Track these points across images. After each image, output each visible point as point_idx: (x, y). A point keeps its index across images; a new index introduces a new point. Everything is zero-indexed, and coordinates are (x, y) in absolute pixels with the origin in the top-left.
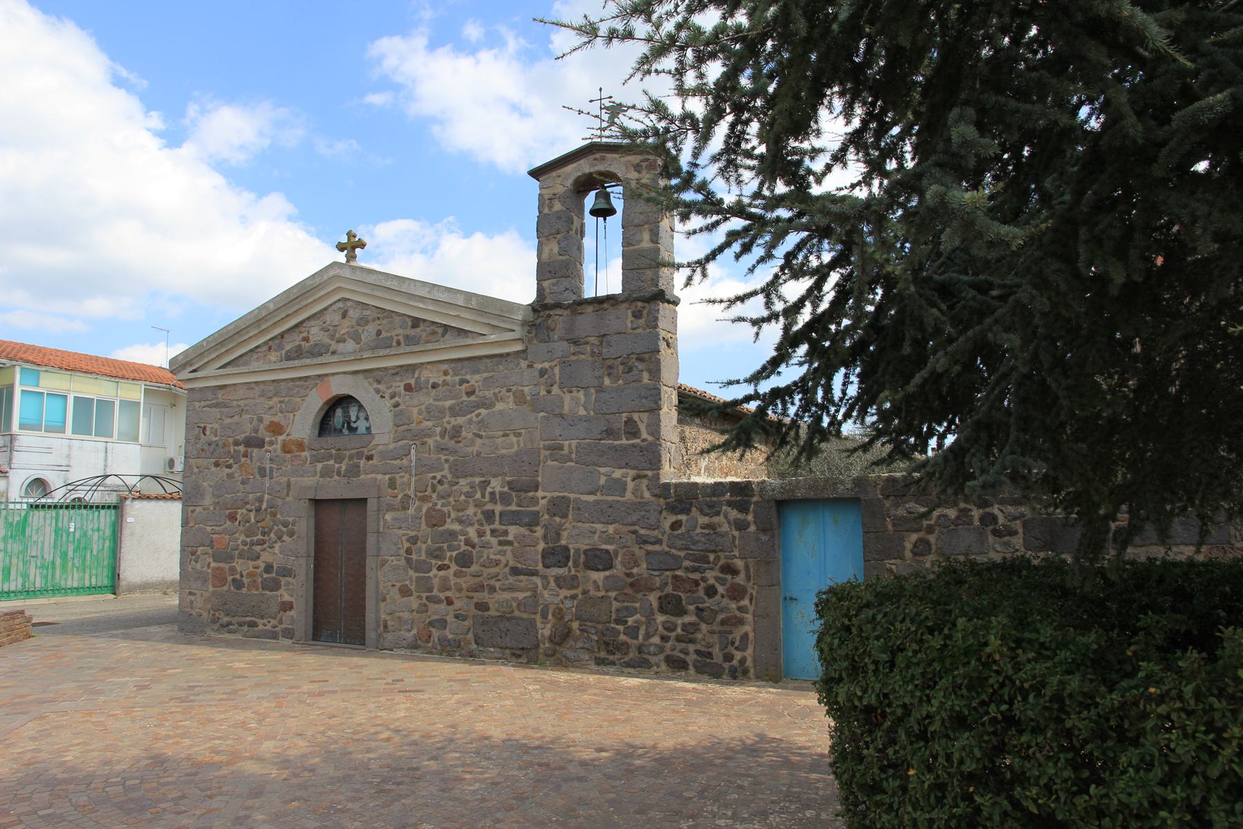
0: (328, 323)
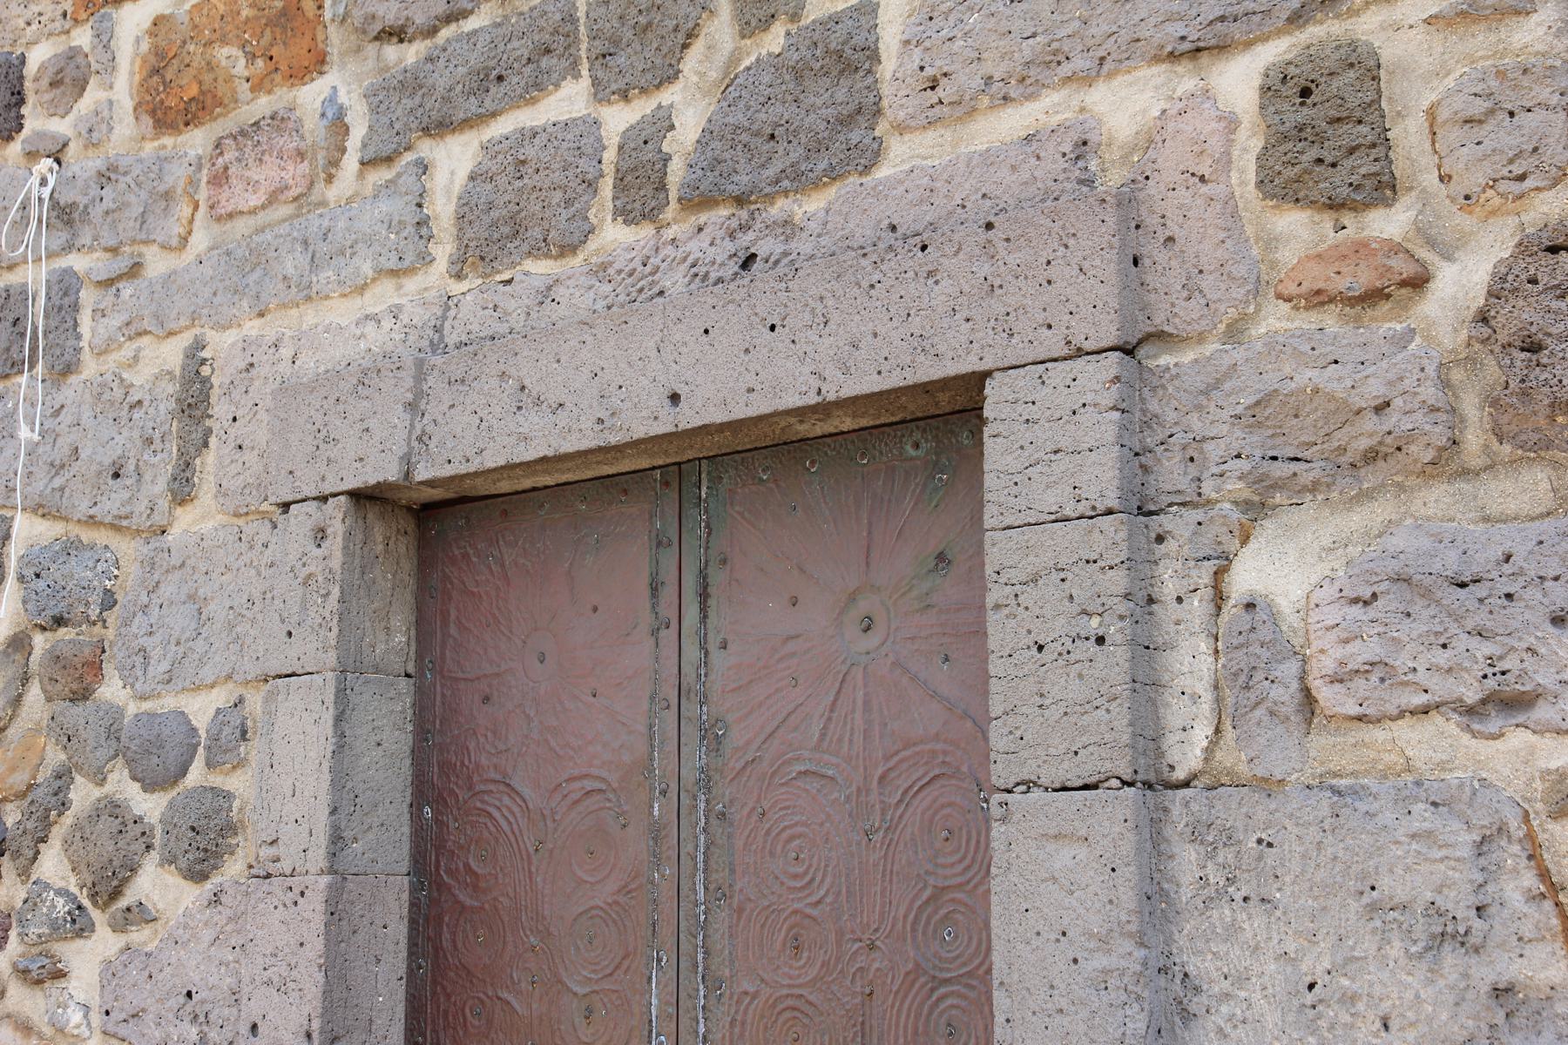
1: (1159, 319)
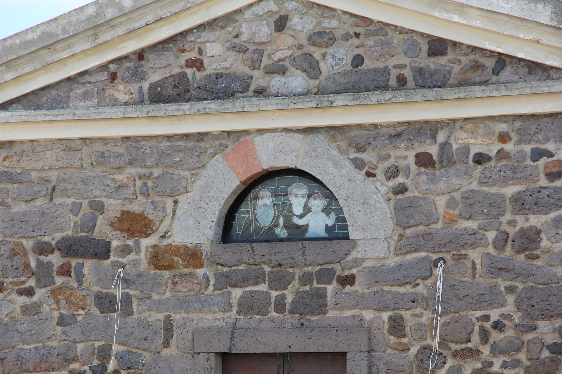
0: (244, 37)
1: (373, 348)
